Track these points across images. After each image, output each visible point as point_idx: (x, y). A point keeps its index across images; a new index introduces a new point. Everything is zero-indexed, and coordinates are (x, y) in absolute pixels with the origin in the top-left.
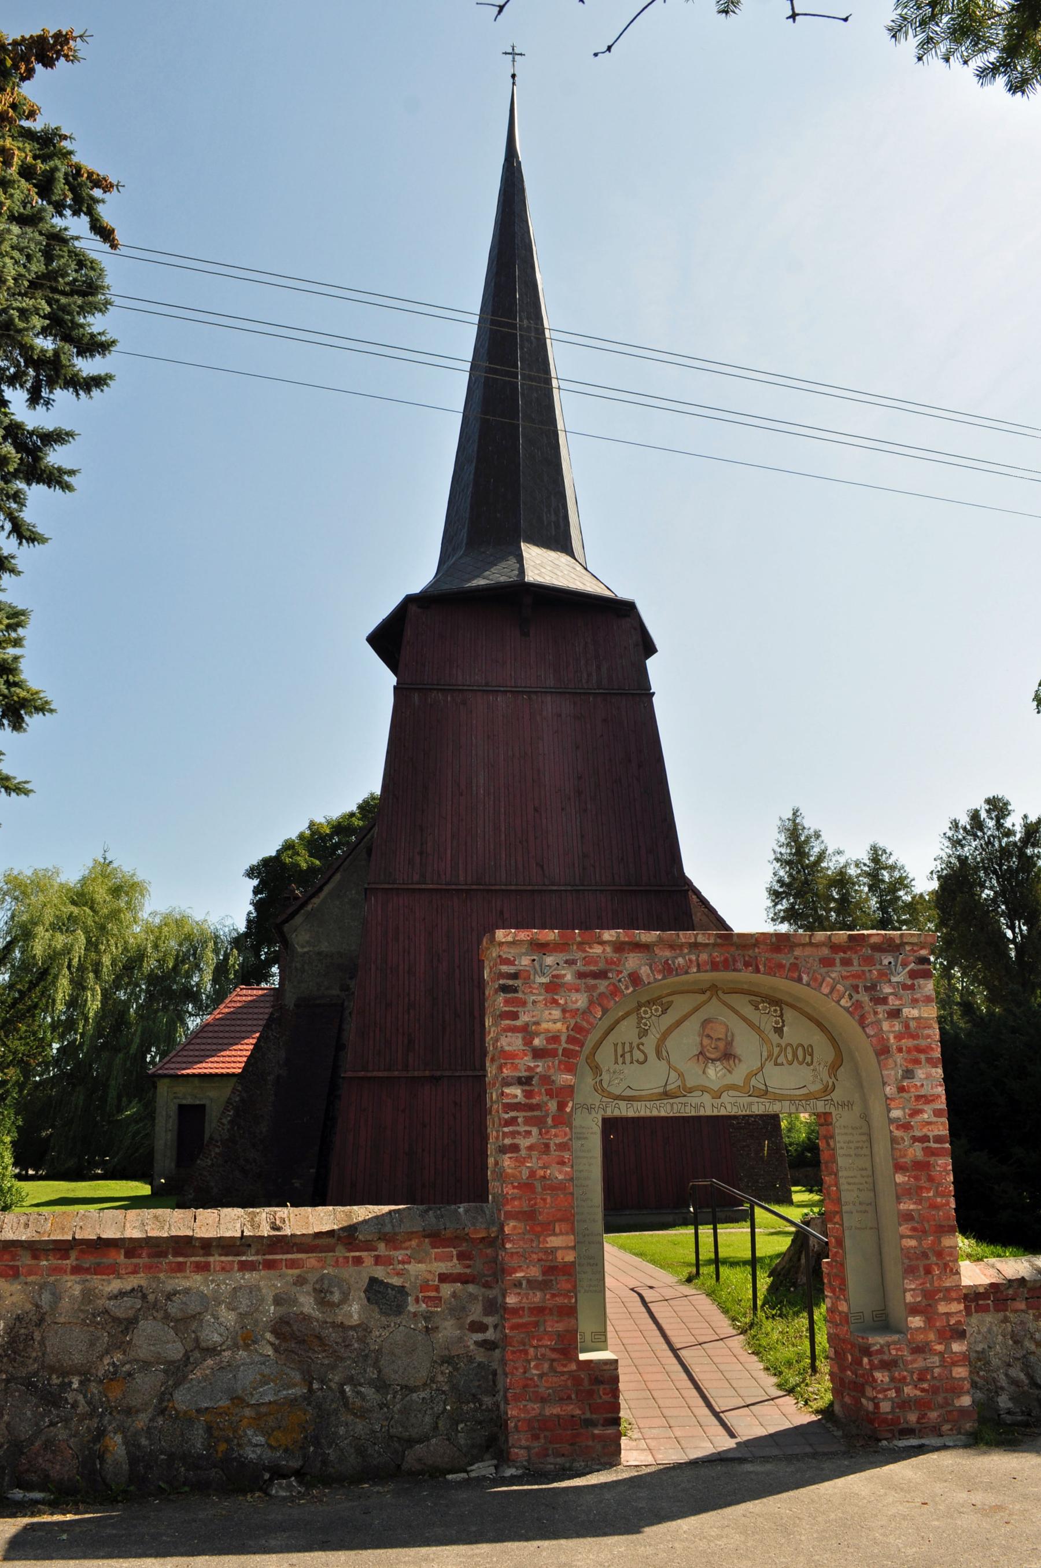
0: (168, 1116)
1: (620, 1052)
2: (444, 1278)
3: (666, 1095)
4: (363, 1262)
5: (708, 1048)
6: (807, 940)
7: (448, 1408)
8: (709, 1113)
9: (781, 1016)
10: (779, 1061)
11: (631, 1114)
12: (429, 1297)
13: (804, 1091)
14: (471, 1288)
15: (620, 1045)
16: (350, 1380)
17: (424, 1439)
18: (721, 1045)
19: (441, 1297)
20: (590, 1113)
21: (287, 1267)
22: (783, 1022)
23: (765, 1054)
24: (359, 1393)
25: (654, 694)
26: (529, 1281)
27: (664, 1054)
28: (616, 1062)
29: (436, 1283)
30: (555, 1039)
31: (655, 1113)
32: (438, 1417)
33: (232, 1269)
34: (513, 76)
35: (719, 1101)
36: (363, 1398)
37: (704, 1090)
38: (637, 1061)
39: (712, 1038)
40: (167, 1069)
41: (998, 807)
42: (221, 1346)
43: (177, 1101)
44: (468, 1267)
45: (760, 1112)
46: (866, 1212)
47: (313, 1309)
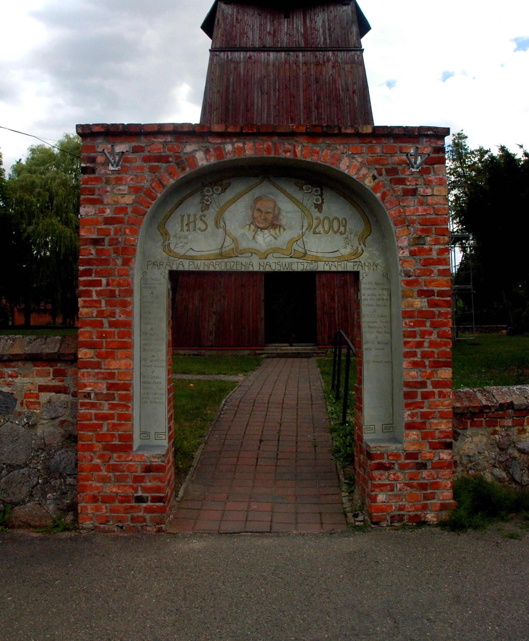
1: (185, 222)
2: (43, 389)
3: (221, 255)
5: (259, 219)
7: (40, 481)
11: (192, 268)
12: (31, 402)
13: (338, 254)
14: (63, 396)
18: (270, 216)
22: (323, 200)
23: (306, 225)
26: (96, 394)
27: (222, 224)
28: (182, 230)
29: (36, 392)
30: (123, 209)
31: (212, 269)
32: (33, 488)
35: (266, 261)
37: (253, 252)
38: (199, 229)
44: (62, 381)
45: (299, 270)
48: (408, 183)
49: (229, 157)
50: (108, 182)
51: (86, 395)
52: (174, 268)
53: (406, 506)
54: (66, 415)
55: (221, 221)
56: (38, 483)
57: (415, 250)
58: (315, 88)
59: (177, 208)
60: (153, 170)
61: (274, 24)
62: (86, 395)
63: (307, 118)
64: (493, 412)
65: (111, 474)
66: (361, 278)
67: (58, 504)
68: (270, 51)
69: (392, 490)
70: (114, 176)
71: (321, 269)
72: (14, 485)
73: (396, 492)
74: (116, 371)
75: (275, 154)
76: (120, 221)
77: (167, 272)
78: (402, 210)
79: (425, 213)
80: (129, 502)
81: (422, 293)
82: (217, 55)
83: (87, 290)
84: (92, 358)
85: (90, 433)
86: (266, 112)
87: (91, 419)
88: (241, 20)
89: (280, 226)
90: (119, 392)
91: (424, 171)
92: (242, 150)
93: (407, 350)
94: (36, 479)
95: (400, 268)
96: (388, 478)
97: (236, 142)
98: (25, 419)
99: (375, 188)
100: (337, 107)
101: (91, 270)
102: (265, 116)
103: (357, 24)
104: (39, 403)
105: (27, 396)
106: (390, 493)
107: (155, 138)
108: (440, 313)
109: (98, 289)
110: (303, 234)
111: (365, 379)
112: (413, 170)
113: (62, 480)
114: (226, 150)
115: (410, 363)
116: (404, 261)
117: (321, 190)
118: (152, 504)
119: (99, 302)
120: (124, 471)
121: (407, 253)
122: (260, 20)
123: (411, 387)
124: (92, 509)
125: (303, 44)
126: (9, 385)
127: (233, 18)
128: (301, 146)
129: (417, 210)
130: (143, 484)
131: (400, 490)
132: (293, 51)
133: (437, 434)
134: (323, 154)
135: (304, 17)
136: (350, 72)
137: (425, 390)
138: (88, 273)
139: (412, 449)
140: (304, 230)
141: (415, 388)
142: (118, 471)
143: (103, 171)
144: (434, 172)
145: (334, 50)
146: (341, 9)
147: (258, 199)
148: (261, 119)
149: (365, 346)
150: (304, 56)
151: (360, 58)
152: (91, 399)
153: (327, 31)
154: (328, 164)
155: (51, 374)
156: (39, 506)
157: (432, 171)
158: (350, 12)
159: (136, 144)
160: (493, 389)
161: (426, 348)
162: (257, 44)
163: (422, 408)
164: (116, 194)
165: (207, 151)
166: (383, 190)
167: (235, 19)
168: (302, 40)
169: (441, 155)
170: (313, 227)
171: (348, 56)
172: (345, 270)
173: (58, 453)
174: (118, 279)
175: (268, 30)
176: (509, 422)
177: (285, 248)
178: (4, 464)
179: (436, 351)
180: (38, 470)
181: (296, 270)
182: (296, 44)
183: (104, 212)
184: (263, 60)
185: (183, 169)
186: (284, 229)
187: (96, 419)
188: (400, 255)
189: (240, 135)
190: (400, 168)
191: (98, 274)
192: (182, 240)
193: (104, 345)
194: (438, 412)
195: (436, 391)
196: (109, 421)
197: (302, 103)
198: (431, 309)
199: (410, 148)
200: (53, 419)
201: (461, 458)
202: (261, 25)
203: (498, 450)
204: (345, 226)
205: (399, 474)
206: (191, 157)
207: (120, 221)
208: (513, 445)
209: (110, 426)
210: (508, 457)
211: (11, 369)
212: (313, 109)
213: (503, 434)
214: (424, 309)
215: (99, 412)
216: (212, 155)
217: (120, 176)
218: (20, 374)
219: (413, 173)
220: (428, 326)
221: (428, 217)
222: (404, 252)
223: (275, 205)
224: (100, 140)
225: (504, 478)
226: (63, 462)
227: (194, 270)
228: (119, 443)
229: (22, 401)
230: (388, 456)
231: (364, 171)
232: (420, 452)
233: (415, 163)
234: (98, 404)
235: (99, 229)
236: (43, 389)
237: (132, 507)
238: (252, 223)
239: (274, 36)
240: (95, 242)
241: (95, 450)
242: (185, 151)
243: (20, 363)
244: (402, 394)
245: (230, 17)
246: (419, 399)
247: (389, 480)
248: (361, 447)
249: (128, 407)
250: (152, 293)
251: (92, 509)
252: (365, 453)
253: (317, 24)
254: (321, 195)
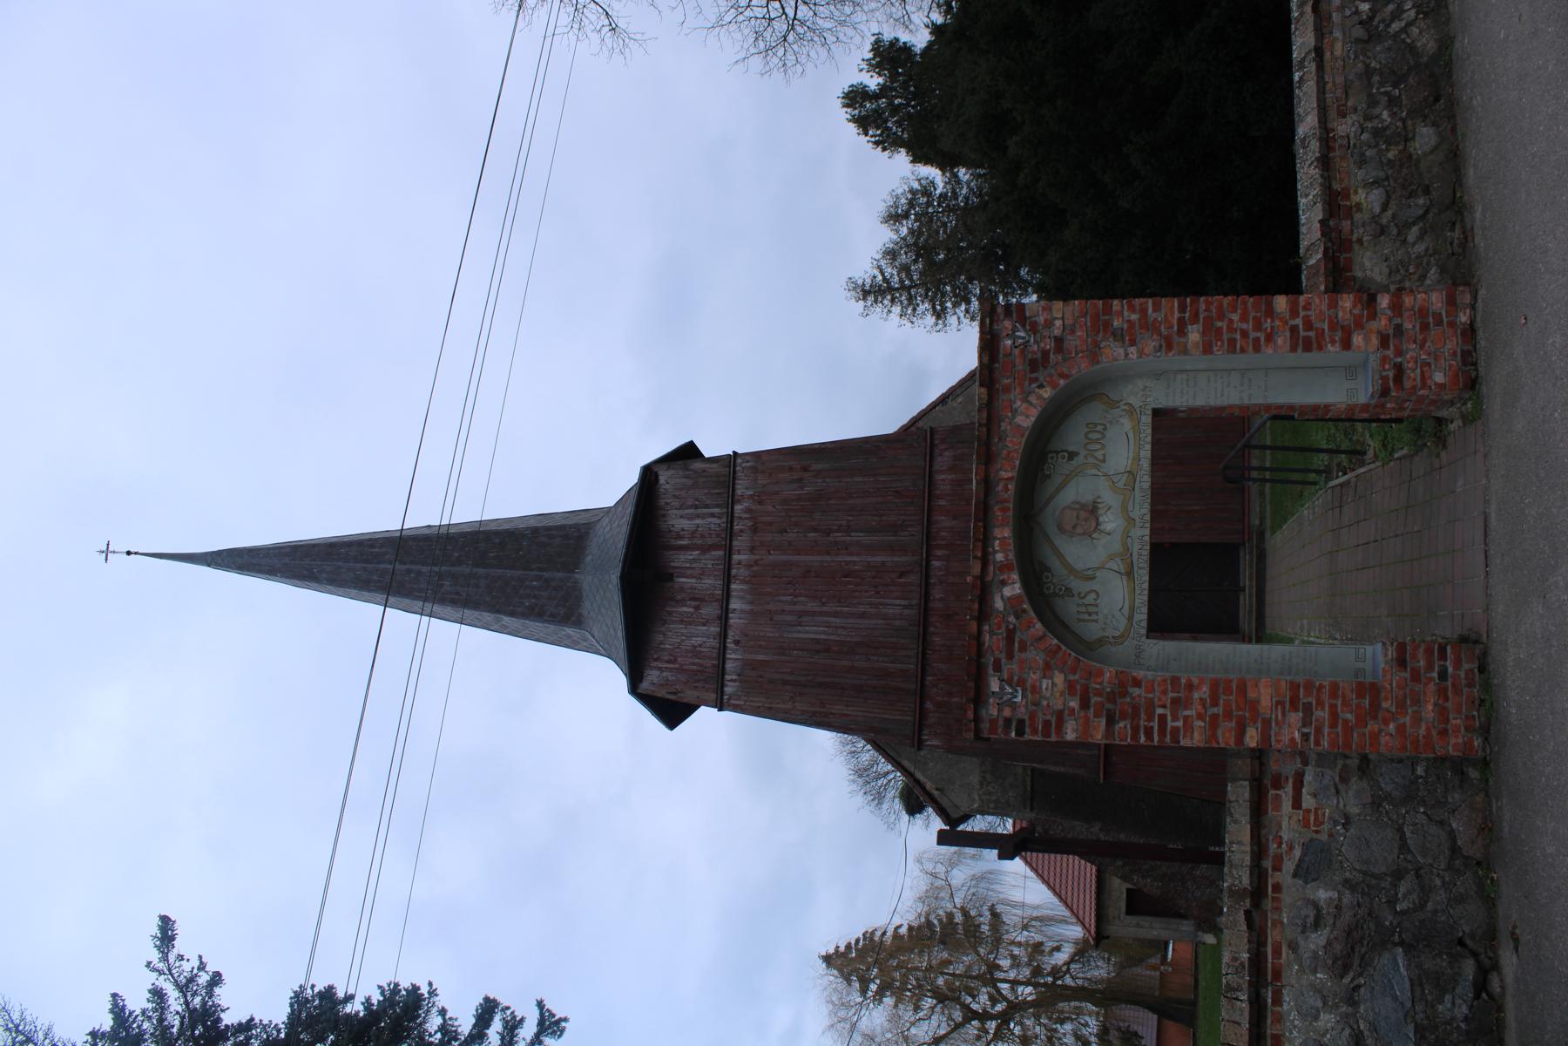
0: (1138, 925)
1: (1086, 617)
2: (1297, 804)
3: (1129, 574)
4: (1278, 883)
5: (1085, 528)
7: (1422, 810)
8: (1147, 532)
9: (1057, 452)
10: (1101, 458)
11: (1145, 610)
12: (1315, 820)
13: (1131, 435)
14: (1308, 778)
15: (1078, 609)
16: (1392, 903)
17: (1452, 835)
18: (1083, 514)
19: (1315, 809)
20: (1144, 650)
21: (1280, 958)
22: (1063, 451)
23: (1094, 471)
24: (1405, 896)
26: (1304, 725)
27: (1090, 572)
28: (1096, 621)
29: (1301, 812)
30: (1071, 686)
31: (1146, 586)
32: (1431, 820)
33: (1279, 1013)
35: (1138, 520)
36: (1409, 892)
37: (1126, 535)
38: (1096, 600)
39: (1076, 524)
40: (1090, 925)
41: (855, 97)
42: (1353, 1030)
43: (1123, 916)
44: (1287, 778)
45: (1149, 480)
46: (1250, 380)
47: (1321, 935)
48: (1048, 347)
49: (1011, 556)
50: (1036, 704)
51: (1305, 738)
52: (1144, 631)
53: (1450, 347)
54: (1331, 775)
55: (1087, 573)
56: (1424, 812)
57: (1129, 340)
58: (795, 535)
59: (1068, 628)
60: (1023, 648)
61: (683, 600)
62: (1305, 738)
63: (846, 549)
64: (1333, 245)
65: (1410, 711)
66: (1160, 406)
67: (1454, 786)
68: (727, 609)
69: (1429, 364)
70: (1030, 695)
71: (1148, 454)
72: (1428, 845)
73: (1431, 360)
74: (1274, 700)
75: (1009, 502)
76: (1085, 690)
77: (1148, 641)
78: (1081, 355)
79: (1084, 328)
80: (1446, 689)
81: (1182, 331)
82: (729, 699)
83: (1171, 732)
84: (1257, 729)
85: (1355, 735)
86: (832, 619)
87: (1337, 734)
88: (671, 655)
89: (1095, 502)
90: (1301, 696)
91: (1034, 328)
92: (1003, 540)
93: (1251, 347)
94: (1419, 816)
95: (1151, 358)
96: (1414, 370)
97: (993, 548)
98: (1338, 828)
99: (1054, 385)
100: (830, 499)
101: (1145, 727)
102: (838, 620)
103: (689, 461)
104: (1316, 809)
105: (1306, 824)
106: (1433, 366)
107: (984, 644)
108: (1206, 310)
109: (1169, 718)
110: (1105, 475)
111: (1287, 401)
112: (1032, 341)
113: (1420, 780)
114: (1003, 559)
115: (1267, 346)
116: (1141, 354)
117: (1051, 452)
118: (1449, 660)
119: (1186, 718)
120: (1405, 693)
121: (1132, 349)
122: (674, 622)
123: (1297, 344)
124: (1457, 737)
125: (721, 553)
126: (1291, 848)
127: (666, 668)
128: (1001, 472)
129: (1079, 337)
130: (1422, 671)
131: (1429, 354)
132: (729, 569)
133: (1356, 312)
134: (1010, 445)
135: (673, 549)
136: (770, 475)
137: (1301, 326)
138: (1149, 732)
139: (1375, 341)
140: (1100, 474)
141: (1298, 339)
142: (1406, 702)
143: (1023, 710)
144: (1035, 316)
145: (732, 500)
146: (664, 487)
147: (1061, 528)
148: (843, 627)
149: (1246, 402)
150: (739, 551)
151: (747, 458)
152: (1310, 733)
153: (699, 511)
154: (1024, 440)
155: (1278, 792)
156: (1456, 813)
157: (1033, 319)
158: (671, 472)
159: (991, 667)
160: (1304, 244)
161: (1248, 326)
162: (715, 629)
163: (1323, 330)
164: (1052, 694)
165: (1004, 583)
166: (1055, 377)
167: (668, 665)
168: (713, 553)
169: (1014, 309)
170: (1097, 462)
171: (743, 478)
172: (1150, 425)
173: (1383, 786)
174: (1157, 694)
175: (691, 610)
176: (1346, 224)
177: (1122, 497)
178: (1398, 858)
179: (1252, 314)
180: (1407, 812)
181: (1149, 484)
182: (717, 565)
183: (1074, 709)
184: (742, 621)
185: (1024, 611)
186: (1099, 497)
187: (1337, 727)
188: (1135, 357)
189: (985, 540)
190: (1030, 356)
191: (1150, 718)
192: (1108, 622)
193: (1241, 713)
194: (1328, 309)
195: (1302, 313)
196: (1339, 710)
197: (819, 558)
198: (1201, 321)
199: (1005, 345)
200: (1337, 792)
201: (1392, 283)
202: (682, 621)
203: (1382, 238)
204: (1096, 425)
205: (1408, 356)
206: (1012, 602)
207: (1085, 690)
208: (1377, 219)
209: (1345, 709)
210: (1392, 224)
211: (1270, 843)
212: (831, 539)
213: (1361, 232)
214: (1201, 329)
215: (1327, 723)
216: (1009, 578)
217: (1029, 689)
218: (1277, 832)
219: (1036, 341)
220: (1222, 324)
221: (1089, 324)
222: (1132, 353)
223: (1068, 507)
224: (983, 712)
225: (1421, 229)
226: (1396, 780)
227: (1147, 607)
228: (1367, 697)
229: (1313, 831)
230: (1385, 370)
231: (1033, 399)
232: (1379, 333)
233: (1023, 338)
234: (1317, 723)
235: (1095, 716)
236: (1297, 804)
237: (1453, 685)
238: (1090, 536)
239: (702, 600)
240: (1111, 722)
241: (1376, 730)
242: (1001, 609)
243: (1264, 832)
244: (1307, 355)
245: (665, 674)
246: (1312, 334)
247: (1416, 369)
248: (1376, 406)
249: (1321, 686)
250: (1175, 660)
251: (1457, 737)
252: (1383, 399)
253: (686, 527)
254: (1057, 452)
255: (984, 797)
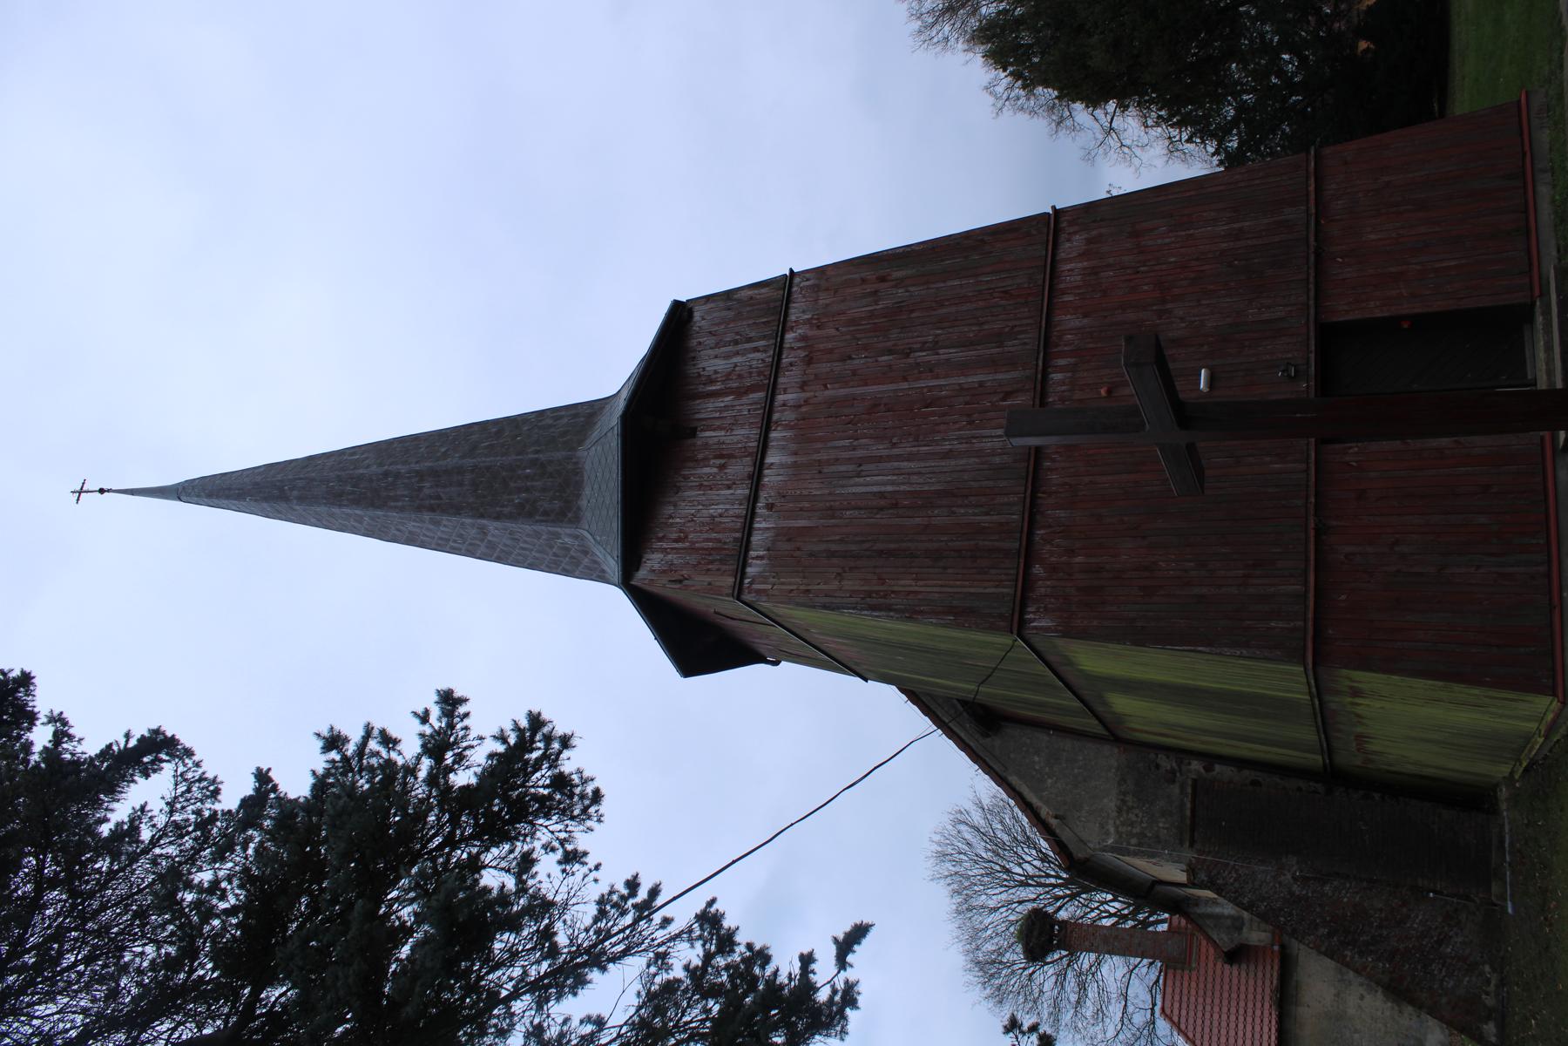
6: (1305, 396)
25: (1054, 207)
34: (102, 491)
255: (1122, 829)
